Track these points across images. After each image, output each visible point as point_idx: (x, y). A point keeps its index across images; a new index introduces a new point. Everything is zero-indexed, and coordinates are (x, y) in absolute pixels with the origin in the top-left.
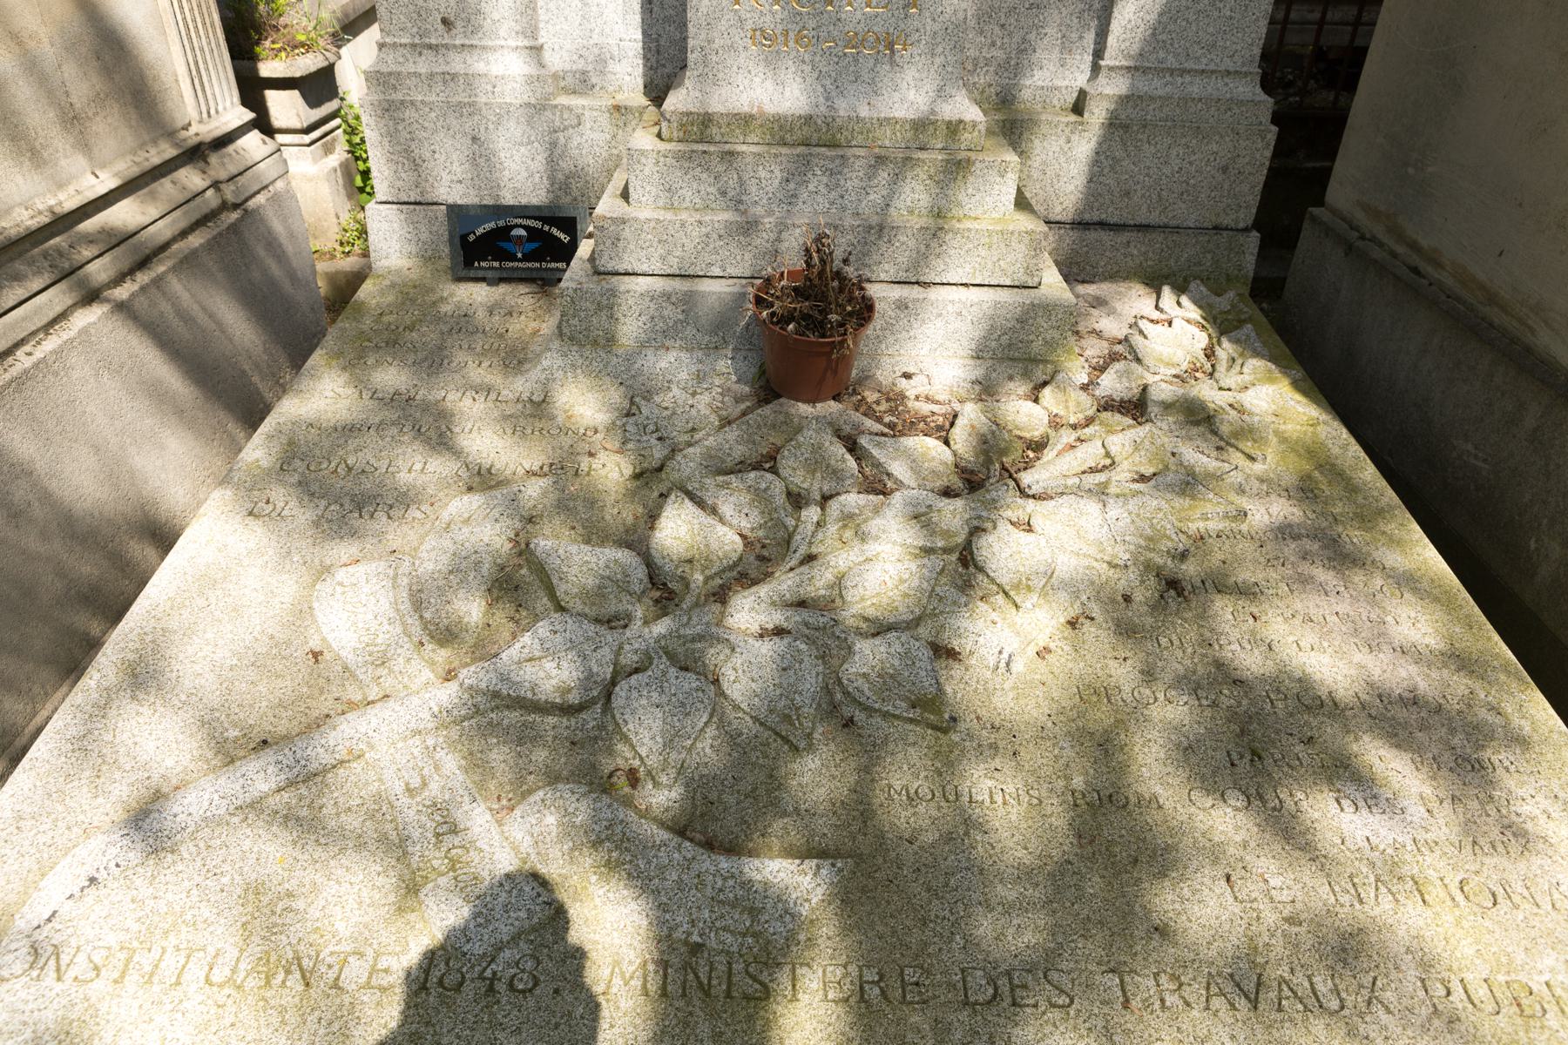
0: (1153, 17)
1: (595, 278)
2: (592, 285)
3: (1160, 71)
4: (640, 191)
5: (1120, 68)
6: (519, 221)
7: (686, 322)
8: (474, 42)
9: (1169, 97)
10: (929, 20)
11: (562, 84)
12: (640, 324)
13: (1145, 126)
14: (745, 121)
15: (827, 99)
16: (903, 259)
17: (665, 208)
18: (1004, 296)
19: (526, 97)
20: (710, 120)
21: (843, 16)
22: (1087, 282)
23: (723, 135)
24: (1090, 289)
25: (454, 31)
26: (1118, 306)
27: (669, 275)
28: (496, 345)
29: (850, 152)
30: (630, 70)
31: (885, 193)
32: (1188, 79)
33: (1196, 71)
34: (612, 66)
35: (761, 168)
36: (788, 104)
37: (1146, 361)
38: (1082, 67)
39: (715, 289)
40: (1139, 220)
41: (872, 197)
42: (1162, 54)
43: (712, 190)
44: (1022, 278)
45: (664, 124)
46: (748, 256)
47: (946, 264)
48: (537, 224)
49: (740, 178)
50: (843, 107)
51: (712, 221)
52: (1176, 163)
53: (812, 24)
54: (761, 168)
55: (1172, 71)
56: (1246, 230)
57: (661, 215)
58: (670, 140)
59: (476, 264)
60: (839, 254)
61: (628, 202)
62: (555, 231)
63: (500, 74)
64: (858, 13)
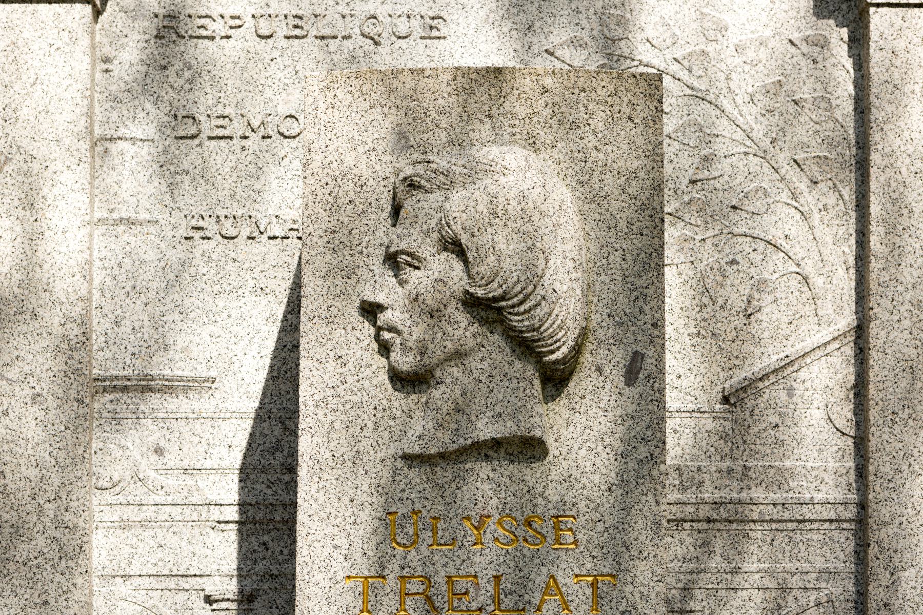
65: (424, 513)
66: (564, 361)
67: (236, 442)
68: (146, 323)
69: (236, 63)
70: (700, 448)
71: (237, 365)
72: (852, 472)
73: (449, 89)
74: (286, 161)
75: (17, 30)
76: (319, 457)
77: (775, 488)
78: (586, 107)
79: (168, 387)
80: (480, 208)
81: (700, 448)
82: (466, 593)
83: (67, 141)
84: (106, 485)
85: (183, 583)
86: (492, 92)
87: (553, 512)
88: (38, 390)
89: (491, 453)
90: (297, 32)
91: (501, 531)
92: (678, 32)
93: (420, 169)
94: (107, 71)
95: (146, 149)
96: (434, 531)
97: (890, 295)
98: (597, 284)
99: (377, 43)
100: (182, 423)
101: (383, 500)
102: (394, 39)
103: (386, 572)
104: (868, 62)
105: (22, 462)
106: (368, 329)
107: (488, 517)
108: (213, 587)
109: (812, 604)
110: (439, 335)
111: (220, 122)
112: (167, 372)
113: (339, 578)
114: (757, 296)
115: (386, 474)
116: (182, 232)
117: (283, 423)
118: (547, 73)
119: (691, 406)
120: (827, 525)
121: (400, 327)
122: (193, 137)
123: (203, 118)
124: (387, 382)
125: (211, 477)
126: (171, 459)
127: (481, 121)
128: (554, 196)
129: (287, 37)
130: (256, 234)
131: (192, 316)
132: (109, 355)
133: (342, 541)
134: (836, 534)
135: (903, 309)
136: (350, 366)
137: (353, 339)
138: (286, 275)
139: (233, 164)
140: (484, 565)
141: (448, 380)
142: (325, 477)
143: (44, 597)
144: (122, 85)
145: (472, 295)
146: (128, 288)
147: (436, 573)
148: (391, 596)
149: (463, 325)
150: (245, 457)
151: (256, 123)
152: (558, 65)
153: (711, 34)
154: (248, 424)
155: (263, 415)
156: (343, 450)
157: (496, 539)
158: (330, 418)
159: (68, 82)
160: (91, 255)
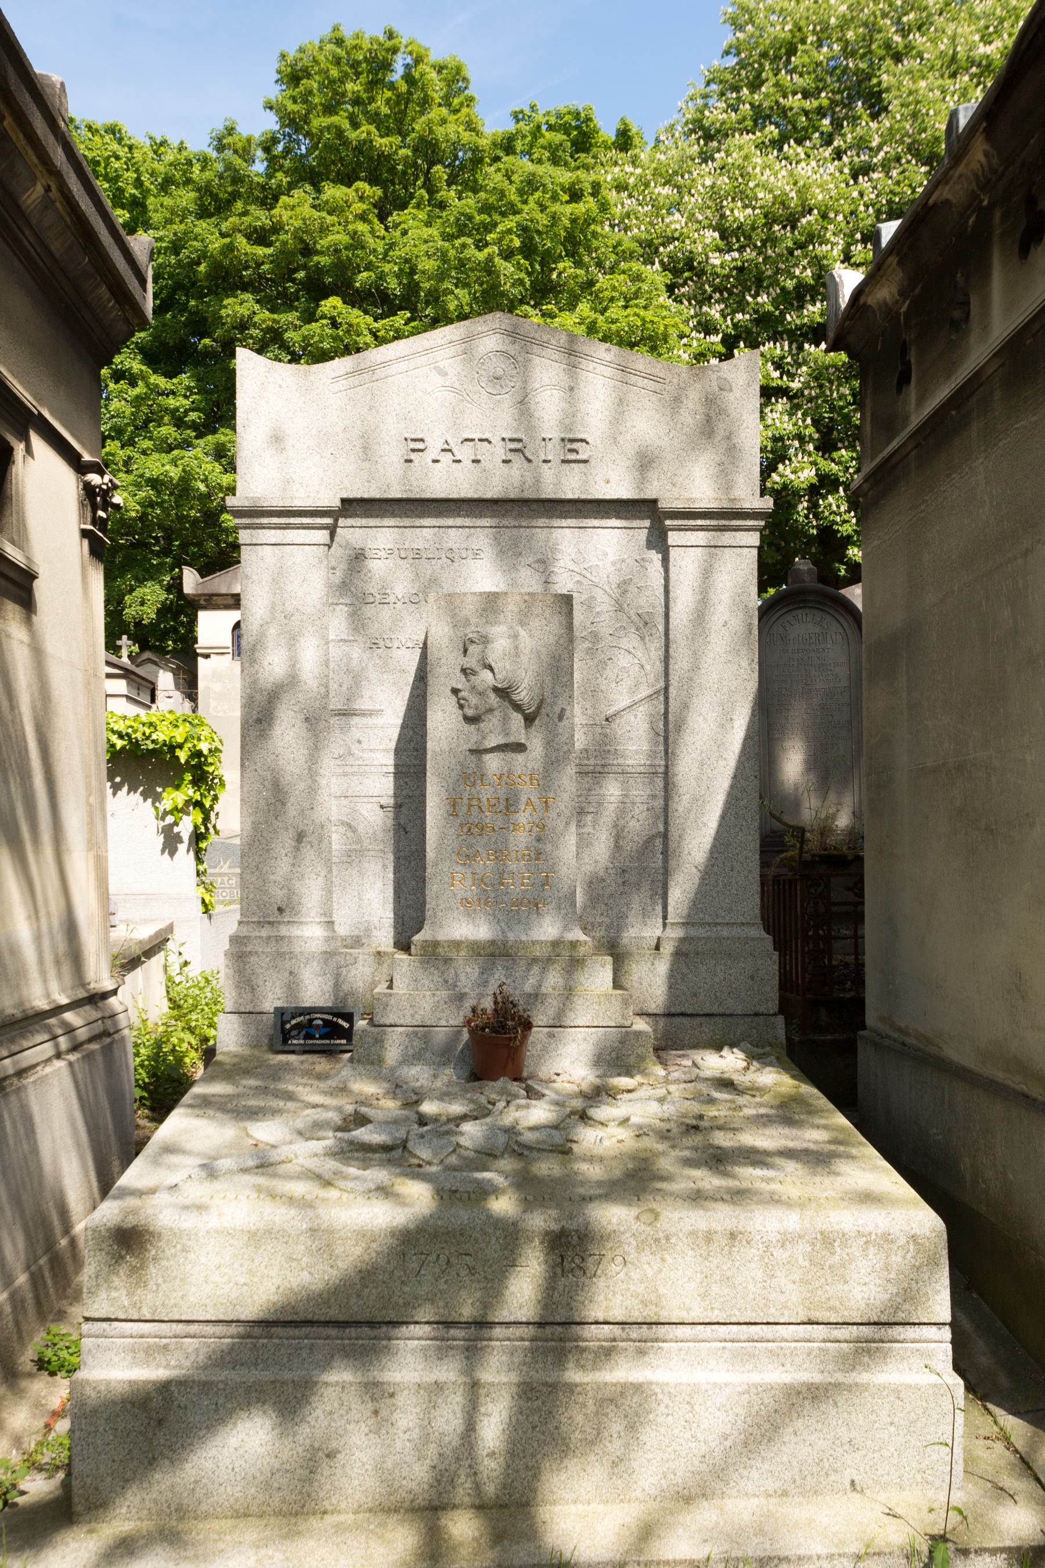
0: (692, 895)
3: (702, 924)
7: (425, 1049)
9: (709, 938)
14: (457, 944)
16: (551, 1012)
34: (375, 933)
39: (440, 1035)
40: (706, 1011)
48: (330, 1017)
50: (511, 936)
52: (721, 976)
53: (493, 895)
55: (709, 924)
56: (775, 1014)
62: (340, 1021)
79: (363, 714)
126: (364, 745)
154: (398, 730)
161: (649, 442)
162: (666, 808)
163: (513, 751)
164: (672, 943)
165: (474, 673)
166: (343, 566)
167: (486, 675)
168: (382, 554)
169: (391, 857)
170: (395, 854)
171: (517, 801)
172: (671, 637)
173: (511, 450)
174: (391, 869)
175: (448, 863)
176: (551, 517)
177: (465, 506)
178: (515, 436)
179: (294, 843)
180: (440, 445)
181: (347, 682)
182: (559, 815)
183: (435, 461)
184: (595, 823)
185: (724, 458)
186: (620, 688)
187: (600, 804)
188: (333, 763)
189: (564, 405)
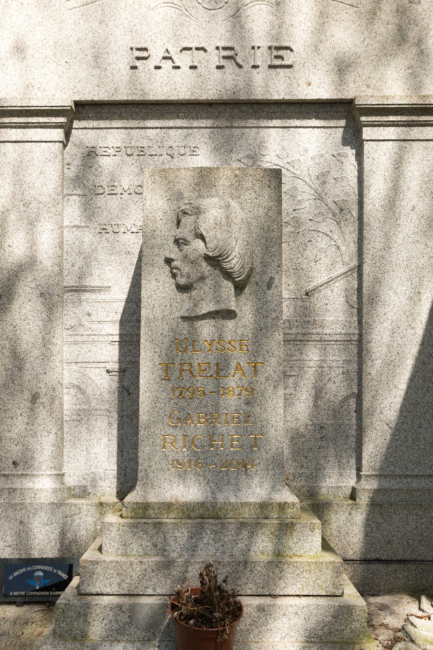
0: (384, 450)
1: (79, 597)
2: (75, 602)
3: (394, 476)
4: (108, 546)
5: (372, 475)
6: (40, 567)
8: (28, 473)
10: (264, 453)
11: (73, 493)
12: (103, 625)
13: (391, 505)
15: (213, 494)
17: (122, 555)
18: (322, 601)
19: (52, 500)
20: (149, 506)
21: (219, 452)
22: (376, 595)
23: (156, 514)
24: (379, 600)
25: (18, 468)
26: (396, 609)
27: (122, 595)
28: (14, 642)
29: (226, 521)
30: (109, 485)
31: (247, 543)
32: (409, 480)
33: (413, 476)
34: (100, 483)
35: (176, 531)
36: (191, 497)
37: (417, 641)
38: (352, 476)
40: (399, 557)
41: (239, 546)
42: (392, 468)
43: (148, 544)
44: (331, 590)
45: (124, 509)
46: (169, 582)
47: (286, 583)
49: (165, 537)
50: (221, 498)
51: (148, 561)
53: (202, 457)
54: (176, 531)
55: (400, 476)
57: (119, 559)
58: (127, 518)
59: (11, 594)
60: (220, 579)
61: (101, 552)
63: (39, 488)
64: (227, 451)
65: (189, 339)
66: (243, 280)
67: (118, 311)
68: (84, 266)
69: (118, 165)
70: (297, 313)
71: (119, 281)
72: (356, 322)
73: (199, 176)
74: (138, 203)
75: (34, 153)
76: (149, 317)
77: (326, 328)
78: (252, 182)
79: (93, 290)
80: (211, 221)
81: (297, 313)
82: (205, 370)
83: (53, 196)
84: (69, 327)
85: (98, 365)
86: (216, 177)
87: (239, 339)
88: (42, 291)
89: (215, 316)
90: (142, 153)
91: (219, 346)
92: (289, 152)
93: (188, 207)
94: (69, 169)
95: (84, 198)
96: (193, 346)
97: (371, 253)
98: (256, 251)
99: (172, 157)
100: (98, 304)
101: (173, 334)
102: (179, 155)
103: (175, 362)
104: (363, 163)
105: (36, 319)
106: (168, 268)
107: (214, 340)
108: (110, 366)
109: (341, 373)
110: (195, 271)
111: (112, 188)
112: (92, 284)
113: (156, 364)
114: (319, 254)
115: (175, 324)
116: (98, 230)
117: (136, 303)
118: (237, 169)
119: (294, 297)
120: (346, 343)
121: (180, 268)
122: (102, 194)
123: (106, 187)
124: (175, 289)
125: (109, 324)
126: (94, 318)
127: (211, 188)
128: (239, 217)
129: (138, 155)
130: (126, 231)
131: (101, 263)
132: (70, 278)
133: (158, 350)
134: (350, 346)
135: (376, 259)
136: (161, 282)
137: (162, 272)
138: (138, 247)
139: (117, 204)
140: (212, 359)
141: (199, 288)
142: (151, 325)
143: (44, 371)
144: (75, 174)
145: (207, 255)
146: (77, 252)
147: (194, 362)
148: (177, 371)
149: (204, 267)
150: (122, 316)
151: (126, 189)
152: (243, 166)
153: (302, 153)
154: (123, 304)
155: (128, 301)
156: (158, 315)
157: (217, 349)
158: (153, 303)
159: (54, 173)
160: (63, 239)
161: (346, 49)
162: (360, 372)
163: (224, 318)
164: (367, 494)
165: (186, 242)
166: (77, 162)
167: (199, 245)
168: (111, 152)
169: (115, 415)
170: (119, 413)
171: (228, 365)
172: (365, 220)
173: (224, 57)
174: (116, 426)
175: (160, 426)
176: (258, 118)
177: (183, 109)
178: (227, 45)
179: (28, 404)
180: (162, 54)
181: (80, 262)
182: (267, 379)
183: (158, 68)
184: (296, 385)
185: (413, 63)
186: (318, 266)
187: (301, 368)
188: (65, 332)
189: (270, 17)
